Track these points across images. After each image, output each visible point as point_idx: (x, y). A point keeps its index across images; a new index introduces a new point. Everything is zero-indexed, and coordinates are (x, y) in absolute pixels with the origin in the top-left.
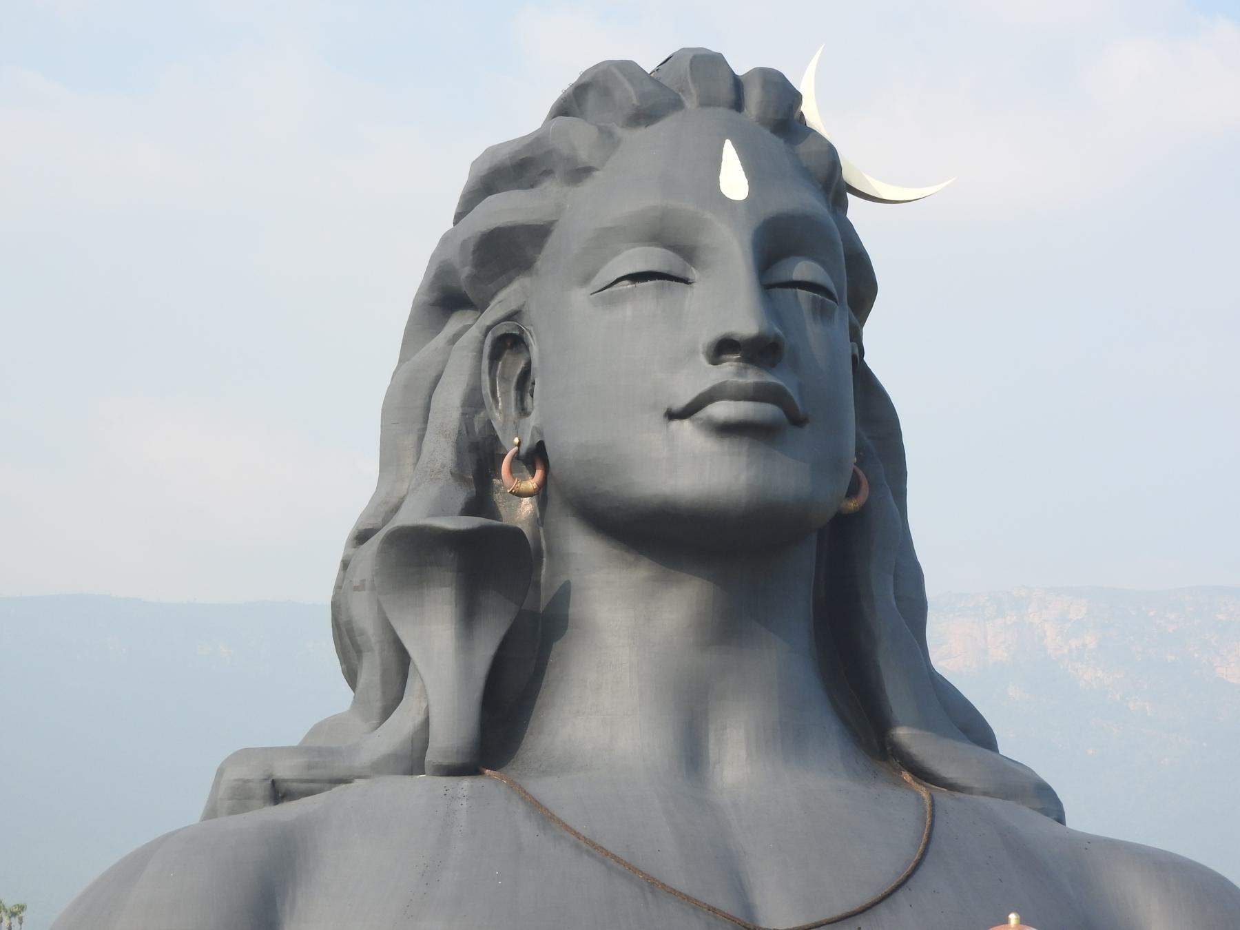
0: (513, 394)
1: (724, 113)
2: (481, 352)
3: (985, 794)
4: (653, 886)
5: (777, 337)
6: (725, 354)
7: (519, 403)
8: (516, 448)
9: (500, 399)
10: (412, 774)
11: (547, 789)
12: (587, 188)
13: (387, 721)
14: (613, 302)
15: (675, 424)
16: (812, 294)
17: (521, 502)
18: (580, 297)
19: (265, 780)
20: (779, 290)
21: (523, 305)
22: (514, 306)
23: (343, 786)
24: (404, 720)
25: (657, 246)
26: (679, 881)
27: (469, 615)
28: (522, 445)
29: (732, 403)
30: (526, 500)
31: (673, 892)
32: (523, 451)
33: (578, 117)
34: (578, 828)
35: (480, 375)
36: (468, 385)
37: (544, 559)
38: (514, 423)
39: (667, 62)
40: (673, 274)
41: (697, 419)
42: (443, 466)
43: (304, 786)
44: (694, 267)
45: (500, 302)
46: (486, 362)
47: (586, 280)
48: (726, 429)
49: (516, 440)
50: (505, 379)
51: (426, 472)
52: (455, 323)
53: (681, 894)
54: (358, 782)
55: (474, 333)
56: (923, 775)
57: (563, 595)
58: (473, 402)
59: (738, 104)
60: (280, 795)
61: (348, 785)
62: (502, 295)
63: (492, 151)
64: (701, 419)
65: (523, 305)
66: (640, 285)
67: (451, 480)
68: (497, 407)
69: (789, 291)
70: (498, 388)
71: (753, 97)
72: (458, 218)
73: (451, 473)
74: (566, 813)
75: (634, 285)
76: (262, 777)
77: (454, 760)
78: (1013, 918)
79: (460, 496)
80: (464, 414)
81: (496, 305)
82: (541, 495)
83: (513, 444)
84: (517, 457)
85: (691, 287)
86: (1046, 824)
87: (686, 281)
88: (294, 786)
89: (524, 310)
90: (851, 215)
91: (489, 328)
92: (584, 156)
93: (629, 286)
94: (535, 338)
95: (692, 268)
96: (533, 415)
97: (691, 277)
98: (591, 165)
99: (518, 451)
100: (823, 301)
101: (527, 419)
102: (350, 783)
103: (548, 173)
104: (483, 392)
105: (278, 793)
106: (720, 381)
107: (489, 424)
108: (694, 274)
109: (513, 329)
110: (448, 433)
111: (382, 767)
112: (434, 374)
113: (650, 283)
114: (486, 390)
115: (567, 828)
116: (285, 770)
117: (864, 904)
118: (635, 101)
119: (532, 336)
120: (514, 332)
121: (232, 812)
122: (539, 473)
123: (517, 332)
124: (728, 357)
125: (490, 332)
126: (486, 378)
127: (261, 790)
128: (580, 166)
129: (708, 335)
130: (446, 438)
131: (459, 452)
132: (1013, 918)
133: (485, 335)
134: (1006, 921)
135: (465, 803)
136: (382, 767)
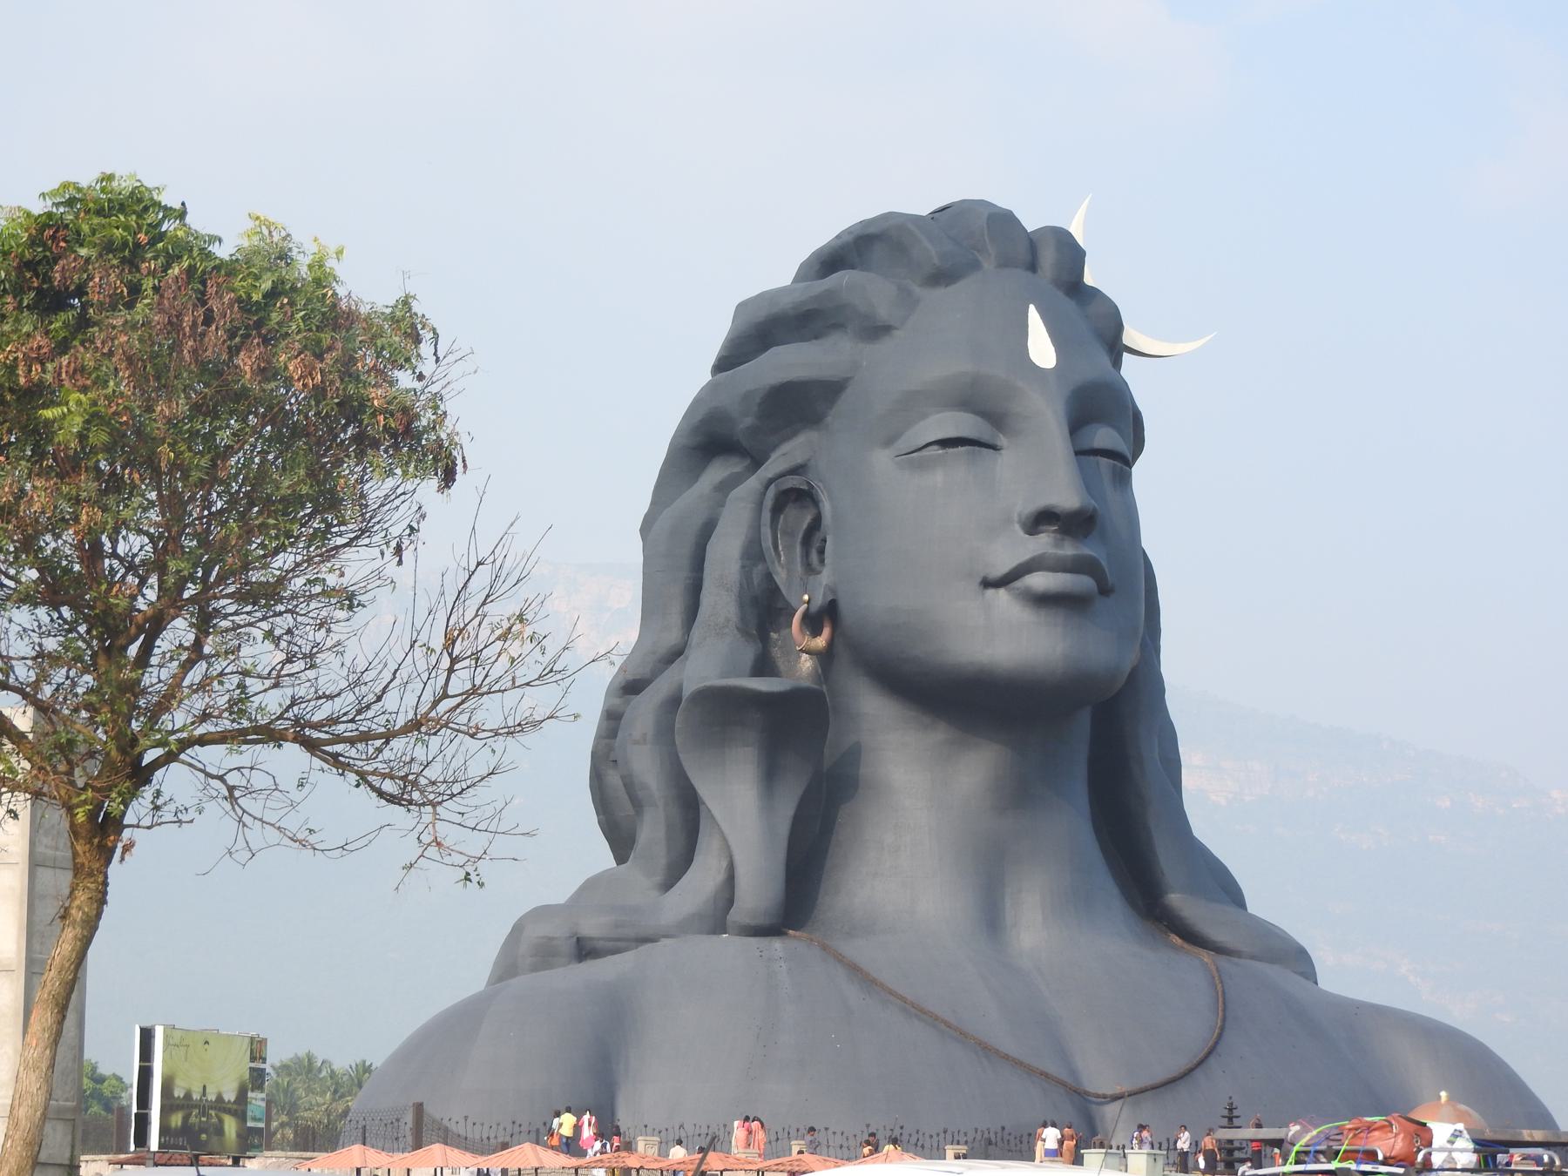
0: (798, 549)
1: (1023, 275)
3: (1253, 958)
4: (986, 1050)
5: (1095, 510)
6: (1043, 525)
8: (806, 605)
9: (782, 553)
11: (859, 950)
12: (884, 347)
14: (921, 466)
15: (990, 592)
16: (1111, 461)
17: (800, 657)
18: (882, 460)
19: (570, 937)
22: (799, 461)
25: (966, 411)
26: (1009, 1046)
27: (770, 775)
28: (812, 602)
29: (1051, 574)
30: (805, 656)
31: (1006, 1057)
33: (853, 268)
38: (801, 579)
39: (944, 212)
40: (982, 441)
41: (1014, 589)
42: (728, 620)
43: (610, 944)
45: (784, 455)
46: (766, 516)
47: (889, 442)
48: (1043, 600)
49: (806, 597)
50: (790, 534)
51: (709, 625)
52: (717, 472)
53: (1014, 1060)
54: (665, 941)
56: (1193, 938)
57: (854, 755)
58: (753, 554)
59: (1033, 267)
60: (584, 953)
62: (786, 447)
65: (809, 460)
66: (951, 450)
67: (739, 636)
68: (779, 561)
71: (1048, 257)
73: (737, 628)
75: (944, 451)
76: (568, 935)
77: (761, 921)
78: (1443, 1094)
79: (748, 653)
80: (743, 567)
82: (825, 658)
83: (803, 601)
86: (1310, 984)
87: (994, 448)
88: (600, 944)
91: (771, 481)
92: (884, 312)
93: (941, 452)
94: (826, 494)
95: (1001, 436)
97: (999, 443)
99: (808, 609)
100: (1122, 468)
101: (819, 576)
102: (656, 942)
103: (838, 326)
105: (584, 950)
106: (1040, 552)
107: (769, 577)
108: (1002, 440)
111: (685, 927)
112: (698, 521)
113: (961, 449)
114: (767, 542)
115: (892, 993)
116: (592, 927)
117: (1182, 1071)
118: (936, 261)
122: (826, 632)
123: (805, 487)
124: (1044, 528)
126: (766, 532)
128: (880, 324)
130: (727, 591)
131: (741, 606)
133: (767, 487)
136: (685, 927)
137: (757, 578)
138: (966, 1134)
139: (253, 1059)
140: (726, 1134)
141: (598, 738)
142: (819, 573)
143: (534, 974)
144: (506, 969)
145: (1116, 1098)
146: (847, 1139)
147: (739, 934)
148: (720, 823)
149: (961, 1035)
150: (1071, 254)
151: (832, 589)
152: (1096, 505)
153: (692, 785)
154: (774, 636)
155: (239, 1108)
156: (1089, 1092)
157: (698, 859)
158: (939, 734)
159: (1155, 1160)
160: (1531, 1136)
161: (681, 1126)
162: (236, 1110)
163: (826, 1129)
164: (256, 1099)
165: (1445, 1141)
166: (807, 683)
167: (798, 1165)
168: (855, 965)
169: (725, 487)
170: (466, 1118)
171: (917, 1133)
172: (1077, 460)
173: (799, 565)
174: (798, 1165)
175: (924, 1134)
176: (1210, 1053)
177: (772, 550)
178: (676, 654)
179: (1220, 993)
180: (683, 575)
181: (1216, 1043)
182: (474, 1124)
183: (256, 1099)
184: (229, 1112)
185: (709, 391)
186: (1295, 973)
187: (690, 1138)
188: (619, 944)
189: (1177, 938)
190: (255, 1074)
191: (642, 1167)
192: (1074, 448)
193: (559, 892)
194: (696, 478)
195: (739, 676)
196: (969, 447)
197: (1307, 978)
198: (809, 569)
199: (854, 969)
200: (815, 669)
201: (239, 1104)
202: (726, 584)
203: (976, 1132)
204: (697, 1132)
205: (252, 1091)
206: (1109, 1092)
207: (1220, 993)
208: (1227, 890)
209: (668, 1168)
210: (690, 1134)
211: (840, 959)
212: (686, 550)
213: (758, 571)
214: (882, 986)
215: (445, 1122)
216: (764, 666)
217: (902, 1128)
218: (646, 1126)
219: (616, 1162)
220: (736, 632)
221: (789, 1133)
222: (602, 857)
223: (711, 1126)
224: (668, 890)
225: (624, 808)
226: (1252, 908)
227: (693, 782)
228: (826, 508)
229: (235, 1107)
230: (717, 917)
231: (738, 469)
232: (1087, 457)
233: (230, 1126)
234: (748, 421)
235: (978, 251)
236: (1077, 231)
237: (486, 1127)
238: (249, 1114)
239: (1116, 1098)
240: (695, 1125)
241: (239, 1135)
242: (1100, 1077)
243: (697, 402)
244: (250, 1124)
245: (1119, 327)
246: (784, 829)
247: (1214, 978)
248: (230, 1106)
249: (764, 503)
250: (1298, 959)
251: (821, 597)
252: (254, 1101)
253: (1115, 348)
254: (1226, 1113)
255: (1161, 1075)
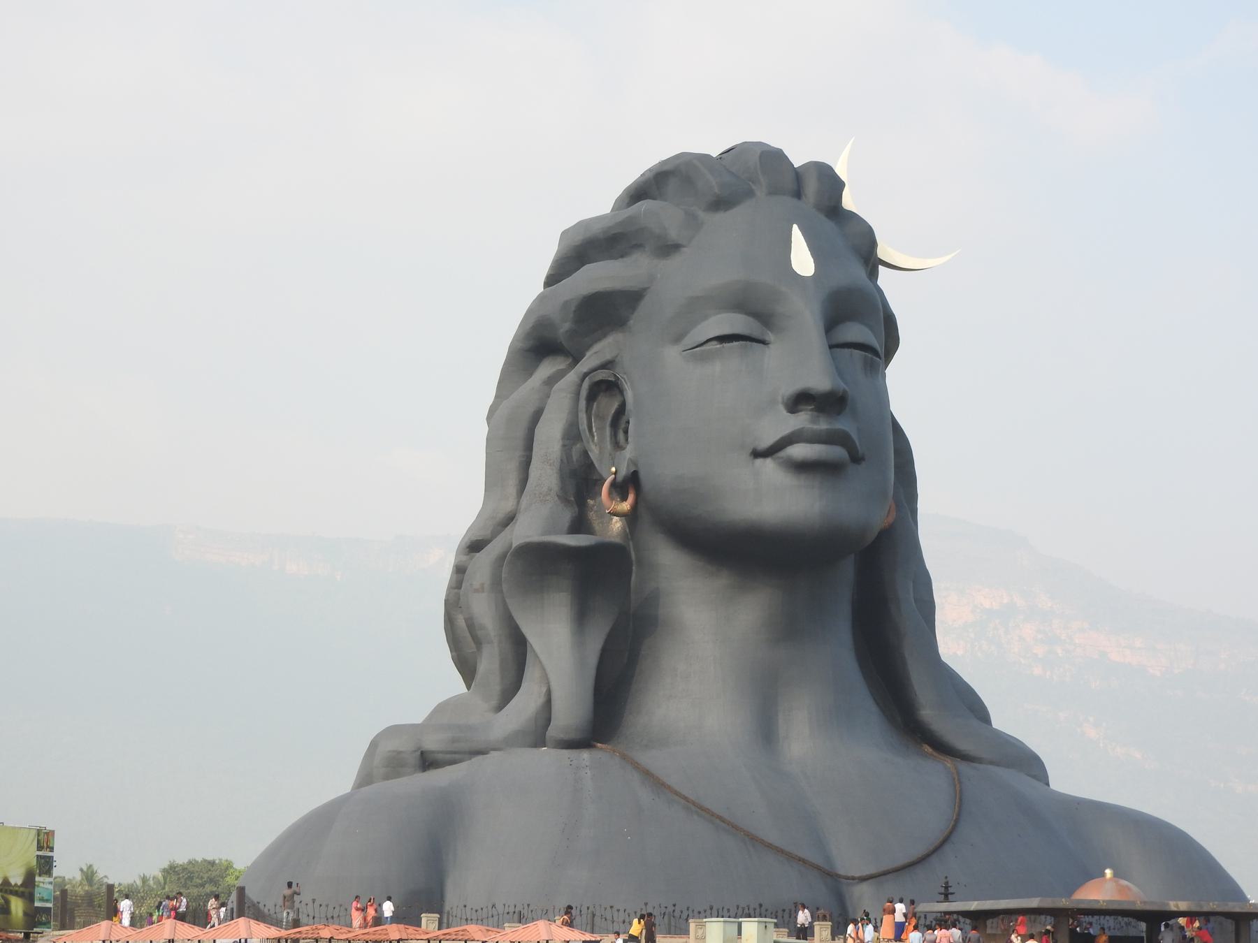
1: (790, 201)
2: (578, 394)
3: (992, 763)
4: (753, 839)
5: (845, 392)
7: (613, 439)
8: (613, 476)
9: (595, 434)
10: (536, 747)
11: (651, 759)
12: (674, 263)
13: (513, 700)
14: (704, 358)
15: (759, 461)
16: (863, 353)
17: (612, 519)
18: (672, 354)
19: (415, 751)
20: (838, 350)
21: (617, 356)
22: (608, 357)
23: (481, 757)
24: (527, 702)
26: (773, 837)
27: (581, 616)
30: (615, 519)
31: (769, 846)
32: (620, 478)
33: (654, 199)
34: (685, 792)
35: (577, 416)
36: (567, 422)
37: (634, 568)
38: (610, 455)
40: (753, 336)
41: (779, 458)
43: (448, 757)
44: (770, 330)
45: (596, 353)
47: (677, 339)
48: (802, 467)
49: (613, 469)
50: (601, 418)
51: (535, 494)
52: (546, 369)
53: (776, 847)
54: (493, 754)
55: (572, 377)
56: (943, 748)
57: (653, 599)
58: (572, 435)
59: (798, 194)
60: (427, 764)
61: (485, 756)
62: (597, 347)
63: (582, 225)
64: (782, 458)
65: (617, 356)
66: (727, 345)
68: (593, 440)
69: (847, 351)
70: (593, 425)
71: (811, 187)
72: (551, 280)
73: (558, 496)
74: (673, 780)
75: (721, 345)
77: (573, 735)
79: (567, 516)
80: (564, 446)
81: (592, 355)
82: (631, 518)
83: (611, 472)
84: (614, 485)
85: (768, 347)
87: (764, 342)
88: (440, 756)
89: (614, 361)
90: (881, 282)
91: (586, 375)
92: (674, 234)
93: (718, 346)
94: (629, 384)
95: (770, 333)
96: (629, 448)
97: (767, 338)
98: (680, 242)
100: (872, 359)
103: (639, 246)
104: (580, 428)
105: (427, 762)
106: (796, 428)
107: (585, 454)
108: (770, 337)
109: (609, 377)
110: (552, 461)
111: (513, 741)
112: (531, 409)
115: (677, 793)
116: (432, 743)
117: (920, 856)
119: (626, 383)
120: (610, 379)
121: (387, 777)
122: (631, 498)
123: (612, 379)
125: (587, 378)
126: (583, 416)
127: (413, 759)
128: (669, 243)
129: (790, 388)
130: (550, 465)
131: (562, 478)
132: (1108, 872)
133: (583, 380)
134: (1103, 875)
135: (589, 772)
136: (513, 741)
137: (575, 455)
138: (729, 910)
139: (40, 848)
140: (530, 911)
141: (450, 588)
142: (624, 449)
143: (386, 782)
144: (365, 778)
145: (863, 879)
146: (629, 916)
147: (555, 747)
148: (539, 655)
149: (733, 828)
150: (830, 183)
151: (633, 462)
152: (847, 388)
153: (517, 624)
154: (591, 502)
155: (27, 889)
156: (840, 875)
157: (524, 685)
158: (722, 581)
159: (766, 927)
160: (1177, 906)
161: (494, 906)
162: (23, 893)
163: (611, 907)
164: (43, 883)
165: (865, 909)
166: (618, 540)
167: (462, 935)
168: (648, 771)
169: (551, 381)
170: (314, 901)
171: (688, 909)
172: (831, 354)
173: (608, 443)
174: (462, 935)
175: (693, 911)
176: (945, 840)
177: (587, 431)
178: (510, 519)
179: (958, 792)
180: (519, 454)
181: (951, 833)
182: (321, 905)
183: (43, 883)
184: (16, 894)
185: (541, 299)
186: (1029, 775)
187: (501, 916)
188: (457, 756)
189: (928, 747)
190: (43, 861)
191: (332, 938)
192: (828, 342)
193: (417, 715)
194: (531, 375)
195: (556, 533)
196: (743, 342)
197: (1039, 780)
198: (617, 446)
199: (647, 775)
200: (623, 528)
201: (26, 887)
202: (550, 460)
203: (738, 909)
204: (506, 911)
205: (40, 875)
206: (857, 875)
207: (958, 792)
208: (976, 709)
209: (354, 938)
210: (501, 912)
211: (636, 766)
212: (520, 433)
213: (576, 451)
214: (669, 788)
215: (261, 906)
216: (579, 525)
217: (674, 905)
218: (465, 906)
219: (312, 934)
220: (556, 498)
221: (581, 911)
222: (455, 684)
223: (267, 905)
224: (501, 710)
225: (470, 647)
226: (996, 723)
227: (517, 622)
228: (629, 395)
229: (21, 889)
230: (537, 734)
231: (562, 366)
232: (843, 350)
233: (17, 907)
234: (566, 326)
235: (753, 182)
236: (841, 171)
237: (331, 908)
238: (37, 895)
239: (863, 879)
240: (504, 905)
241: (25, 914)
242: (849, 861)
243: (529, 312)
244: (37, 904)
245: (873, 244)
246: (593, 660)
247: (954, 779)
248: (17, 889)
249: (581, 393)
250: (1031, 765)
251: (625, 469)
252: (41, 885)
253: (870, 261)
254: (942, 890)
255: (901, 860)
